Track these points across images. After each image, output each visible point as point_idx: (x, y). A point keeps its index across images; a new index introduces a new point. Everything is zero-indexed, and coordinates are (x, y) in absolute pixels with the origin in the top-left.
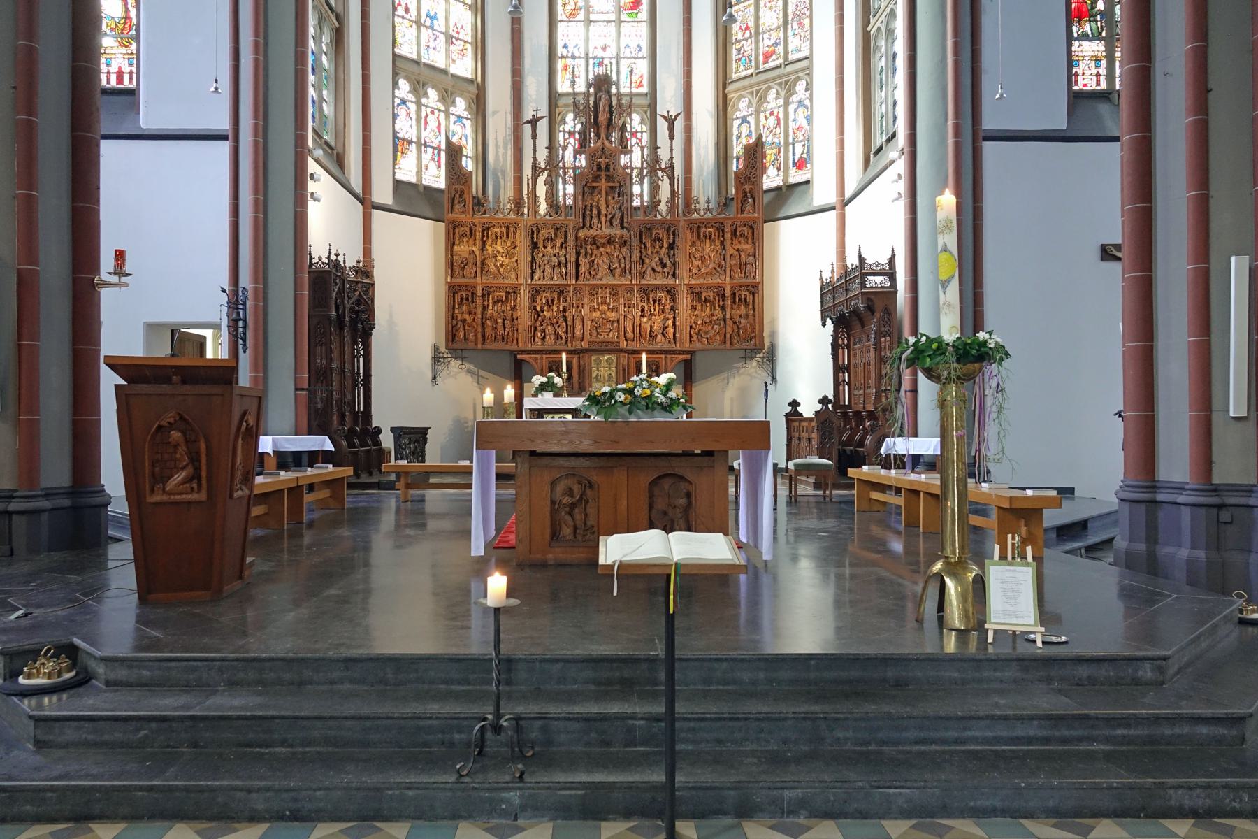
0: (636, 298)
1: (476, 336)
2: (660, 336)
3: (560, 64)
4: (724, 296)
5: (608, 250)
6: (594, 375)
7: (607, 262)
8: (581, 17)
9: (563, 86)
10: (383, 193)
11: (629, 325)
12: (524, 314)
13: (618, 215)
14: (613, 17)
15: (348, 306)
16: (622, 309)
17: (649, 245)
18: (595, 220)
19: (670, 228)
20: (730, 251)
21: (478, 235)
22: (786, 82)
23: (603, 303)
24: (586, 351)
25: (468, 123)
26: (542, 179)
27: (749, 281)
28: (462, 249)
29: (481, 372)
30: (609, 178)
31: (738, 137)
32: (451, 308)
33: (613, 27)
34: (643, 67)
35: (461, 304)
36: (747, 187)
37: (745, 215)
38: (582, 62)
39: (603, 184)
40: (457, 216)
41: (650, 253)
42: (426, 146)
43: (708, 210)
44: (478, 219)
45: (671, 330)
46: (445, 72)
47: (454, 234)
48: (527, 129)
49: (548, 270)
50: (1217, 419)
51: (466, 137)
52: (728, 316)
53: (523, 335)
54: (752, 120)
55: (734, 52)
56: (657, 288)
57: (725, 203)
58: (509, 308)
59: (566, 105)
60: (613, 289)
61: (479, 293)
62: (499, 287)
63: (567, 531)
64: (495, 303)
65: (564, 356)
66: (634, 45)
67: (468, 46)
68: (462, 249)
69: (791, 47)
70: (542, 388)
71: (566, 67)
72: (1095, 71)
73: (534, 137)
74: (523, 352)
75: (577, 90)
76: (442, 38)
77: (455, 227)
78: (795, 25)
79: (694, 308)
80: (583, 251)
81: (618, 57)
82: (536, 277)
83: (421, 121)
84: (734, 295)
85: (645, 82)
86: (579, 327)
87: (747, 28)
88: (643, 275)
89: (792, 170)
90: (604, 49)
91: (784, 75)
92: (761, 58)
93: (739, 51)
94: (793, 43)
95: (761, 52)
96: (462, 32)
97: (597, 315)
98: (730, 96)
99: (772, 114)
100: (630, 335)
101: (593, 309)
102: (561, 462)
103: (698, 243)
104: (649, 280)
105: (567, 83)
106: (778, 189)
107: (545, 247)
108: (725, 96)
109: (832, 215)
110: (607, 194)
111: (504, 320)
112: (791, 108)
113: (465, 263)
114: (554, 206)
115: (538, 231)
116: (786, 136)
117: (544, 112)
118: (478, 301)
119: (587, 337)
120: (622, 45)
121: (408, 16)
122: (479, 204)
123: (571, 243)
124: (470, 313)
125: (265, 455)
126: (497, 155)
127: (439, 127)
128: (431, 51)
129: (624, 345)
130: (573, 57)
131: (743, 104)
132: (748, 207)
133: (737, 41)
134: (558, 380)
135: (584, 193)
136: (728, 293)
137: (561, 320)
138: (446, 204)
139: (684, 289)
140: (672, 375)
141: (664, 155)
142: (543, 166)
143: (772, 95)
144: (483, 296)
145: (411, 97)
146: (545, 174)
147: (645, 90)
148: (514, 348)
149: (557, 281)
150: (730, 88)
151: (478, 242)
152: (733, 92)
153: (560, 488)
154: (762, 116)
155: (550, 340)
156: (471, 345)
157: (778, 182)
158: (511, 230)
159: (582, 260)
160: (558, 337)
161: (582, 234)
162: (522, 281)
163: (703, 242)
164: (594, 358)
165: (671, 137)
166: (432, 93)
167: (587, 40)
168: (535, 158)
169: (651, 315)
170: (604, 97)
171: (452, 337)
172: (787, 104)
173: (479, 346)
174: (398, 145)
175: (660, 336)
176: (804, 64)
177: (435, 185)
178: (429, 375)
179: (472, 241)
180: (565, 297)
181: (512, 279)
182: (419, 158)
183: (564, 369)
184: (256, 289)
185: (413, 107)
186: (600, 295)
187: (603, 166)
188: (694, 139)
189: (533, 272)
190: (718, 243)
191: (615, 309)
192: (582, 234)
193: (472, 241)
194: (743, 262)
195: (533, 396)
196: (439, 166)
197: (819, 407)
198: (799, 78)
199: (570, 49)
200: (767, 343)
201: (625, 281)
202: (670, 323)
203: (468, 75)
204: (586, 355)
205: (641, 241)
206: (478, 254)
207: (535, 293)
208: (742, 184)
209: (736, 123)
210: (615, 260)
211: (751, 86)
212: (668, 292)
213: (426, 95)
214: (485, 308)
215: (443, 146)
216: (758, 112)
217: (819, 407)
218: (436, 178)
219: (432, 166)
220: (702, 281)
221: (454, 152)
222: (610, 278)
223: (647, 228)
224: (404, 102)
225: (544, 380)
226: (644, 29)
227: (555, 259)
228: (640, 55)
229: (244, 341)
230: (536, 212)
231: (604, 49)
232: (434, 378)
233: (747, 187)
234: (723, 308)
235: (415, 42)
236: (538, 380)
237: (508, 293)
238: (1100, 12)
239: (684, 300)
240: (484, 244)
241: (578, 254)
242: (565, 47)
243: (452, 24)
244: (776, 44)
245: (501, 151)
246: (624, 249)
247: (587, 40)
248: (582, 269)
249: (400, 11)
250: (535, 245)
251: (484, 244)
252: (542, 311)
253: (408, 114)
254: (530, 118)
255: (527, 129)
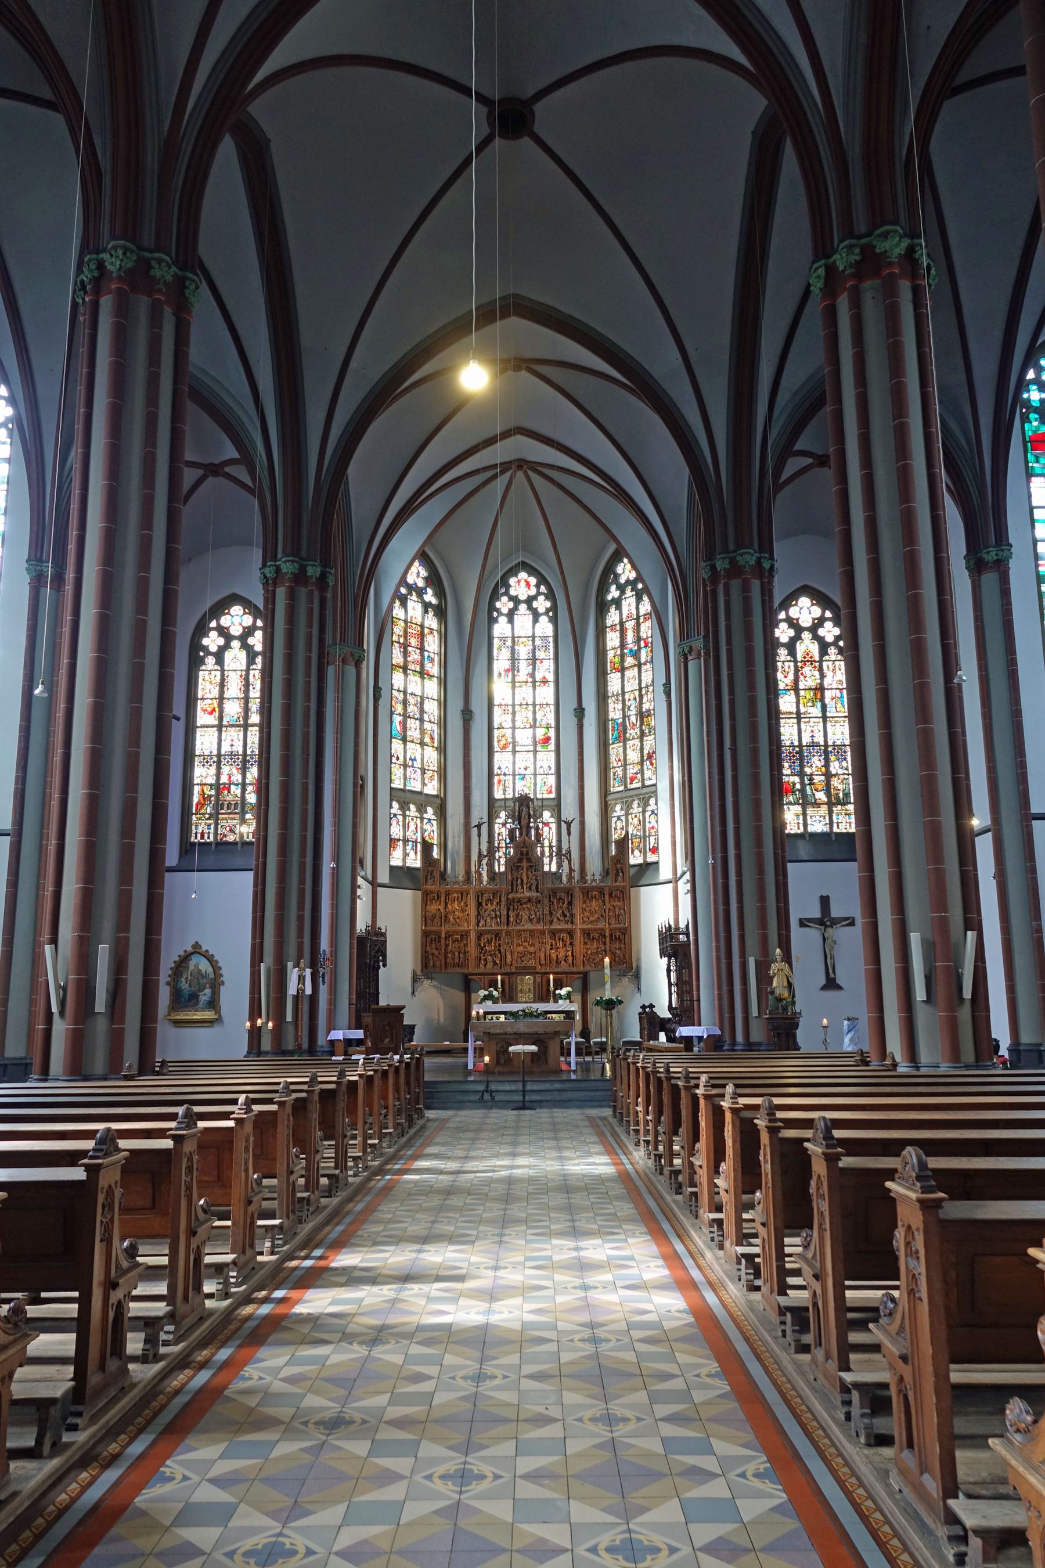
0: (548, 938)
1: (441, 964)
2: (563, 962)
3: (496, 779)
4: (605, 936)
5: (528, 906)
6: (519, 988)
7: (528, 913)
8: (510, 748)
9: (498, 794)
10: (383, 877)
11: (542, 955)
12: (472, 949)
13: (535, 883)
14: (531, 748)
15: (373, 954)
16: (537, 945)
17: (555, 902)
18: (519, 887)
19: (569, 892)
20: (608, 906)
21: (443, 899)
22: (644, 798)
23: (525, 941)
24: (513, 973)
25: (434, 823)
26: (485, 862)
27: (621, 926)
28: (433, 908)
29: (444, 987)
30: (529, 860)
31: (615, 829)
32: (424, 946)
33: (531, 754)
34: (552, 780)
35: (431, 944)
36: (619, 866)
37: (618, 884)
38: (511, 777)
39: (525, 864)
40: (429, 887)
41: (556, 908)
42: (408, 841)
43: (594, 880)
44: (443, 888)
45: (570, 958)
46: (420, 793)
47: (427, 898)
48: (475, 831)
49: (488, 920)
50: (750, 1017)
51: (433, 831)
52: (608, 949)
53: (472, 963)
54: (623, 818)
55: (612, 774)
56: (561, 931)
57: (606, 873)
58: (462, 945)
59: (500, 807)
60: (532, 932)
61: (443, 936)
62: (456, 932)
63: (502, 1061)
64: (453, 942)
65: (499, 977)
66: (546, 766)
67: (435, 773)
68: (433, 908)
69: (646, 776)
70: (486, 998)
71: (499, 781)
72: (796, 822)
73: (479, 835)
74: (473, 974)
75: (508, 797)
76: (419, 771)
77: (427, 894)
78: (648, 762)
79: (585, 943)
80: (512, 907)
81: (535, 775)
82: (481, 925)
83: (405, 827)
84: (611, 935)
85: (553, 790)
86: (509, 957)
87: (619, 760)
88: (551, 922)
89: (649, 854)
90: (526, 769)
91: (642, 794)
92: (628, 780)
93: (614, 774)
94: (648, 774)
95: (628, 776)
96: (431, 765)
97: (521, 948)
98: (609, 802)
99: (636, 816)
100: (543, 962)
101: (519, 945)
102: (499, 1036)
103: (588, 901)
104: (556, 926)
105: (501, 792)
106: (640, 865)
107: (486, 905)
108: (606, 802)
109: (671, 886)
110: (527, 870)
111: (459, 953)
112: (647, 814)
113: (434, 917)
114: (493, 876)
115: (482, 894)
116: (644, 832)
117: (485, 819)
118: (443, 941)
119: (515, 964)
120: (538, 767)
121: (398, 762)
122: (443, 875)
123: (504, 903)
124: (437, 949)
125: (336, 1042)
126: (454, 843)
127: (416, 828)
128: (412, 780)
129: (539, 969)
130: (505, 775)
131: (618, 807)
132: (620, 878)
133: (614, 768)
134: (495, 993)
135: (512, 870)
136: (607, 934)
137: (497, 952)
138: (422, 879)
139: (578, 931)
140: (569, 989)
141: (565, 846)
142: (485, 854)
143: (635, 804)
144: (446, 938)
145: (399, 812)
146: (487, 858)
147: (553, 796)
148: (466, 971)
149: (494, 927)
150: (609, 798)
151: (443, 903)
152: (612, 800)
153: (499, 1046)
154: (630, 817)
155: (490, 965)
156: (437, 970)
157: (640, 861)
158: (464, 894)
159: (511, 914)
160: (495, 963)
161: (510, 896)
162: (471, 928)
163: (591, 900)
164: (519, 978)
165: (569, 834)
166: (412, 807)
167: (514, 763)
168: (480, 849)
169: (557, 948)
170: (525, 809)
171: (425, 964)
172: (644, 812)
173: (443, 970)
174: (393, 842)
175: (563, 962)
176: (653, 789)
177: (414, 866)
178: (410, 991)
179: (438, 903)
180: (500, 938)
181: (464, 927)
182: (405, 849)
183: (500, 986)
184: (331, 951)
185: (400, 818)
186: (523, 936)
187: (525, 852)
188: (587, 829)
189: (479, 922)
190: (601, 901)
191: (533, 945)
192: (510, 896)
193: (438, 903)
194: (617, 913)
195: (479, 1003)
196: (416, 853)
197: (641, 1010)
198: (651, 797)
199: (503, 770)
200: (634, 966)
201: (540, 927)
202: (570, 953)
203: (435, 793)
204: (514, 976)
205: (550, 900)
206: (442, 911)
207: (480, 935)
208: (616, 864)
209: (614, 820)
210: (533, 913)
211: (622, 798)
212: (569, 933)
213: (409, 809)
214: (447, 946)
215: (419, 840)
216: (627, 815)
217: (641, 1010)
218: (415, 861)
219: (412, 854)
220: (590, 926)
221: (427, 847)
222: (530, 924)
223: (554, 892)
224: (395, 815)
225: (487, 993)
226: (552, 756)
227: (493, 913)
228: (550, 772)
229: (323, 978)
230: (481, 882)
231: (526, 769)
232: (413, 992)
233: (619, 866)
234: (605, 944)
235: (402, 777)
236: (483, 993)
237: (462, 935)
238: (798, 790)
239: (578, 937)
240: (446, 904)
241: (508, 909)
242: (499, 768)
243: (425, 761)
244: (636, 773)
245: (457, 840)
246: (539, 906)
247: (514, 763)
248: (511, 919)
249: (394, 760)
250: (480, 904)
251: (446, 904)
252: (485, 946)
253: (398, 823)
254: (477, 824)
255: (475, 831)
